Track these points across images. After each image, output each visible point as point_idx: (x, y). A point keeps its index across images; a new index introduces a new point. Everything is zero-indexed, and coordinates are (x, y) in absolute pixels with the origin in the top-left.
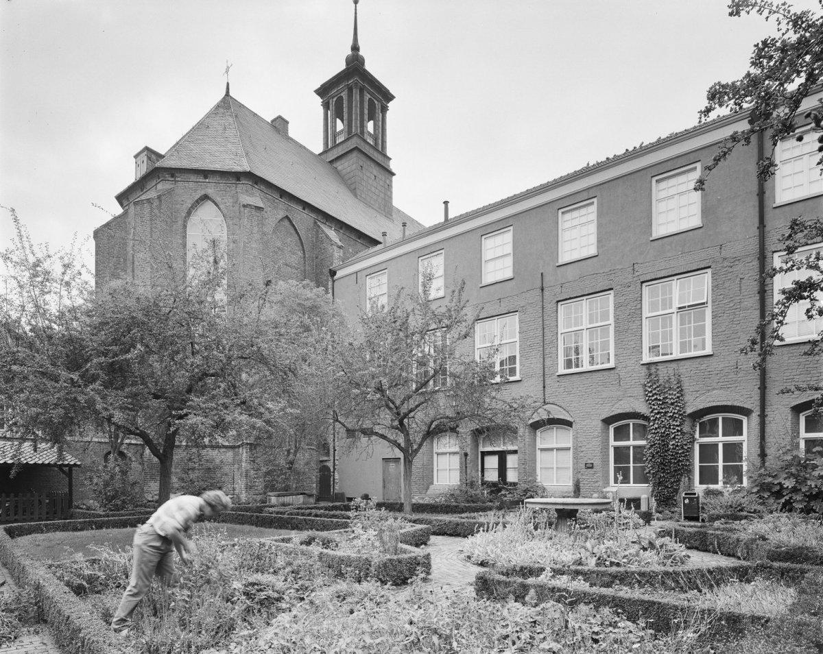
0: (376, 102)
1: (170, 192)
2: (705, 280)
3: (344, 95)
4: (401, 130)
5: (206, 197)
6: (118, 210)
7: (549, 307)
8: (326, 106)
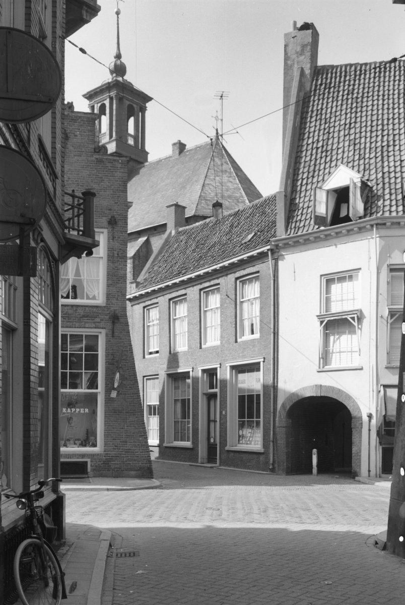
0: (135, 106)
3: (107, 103)
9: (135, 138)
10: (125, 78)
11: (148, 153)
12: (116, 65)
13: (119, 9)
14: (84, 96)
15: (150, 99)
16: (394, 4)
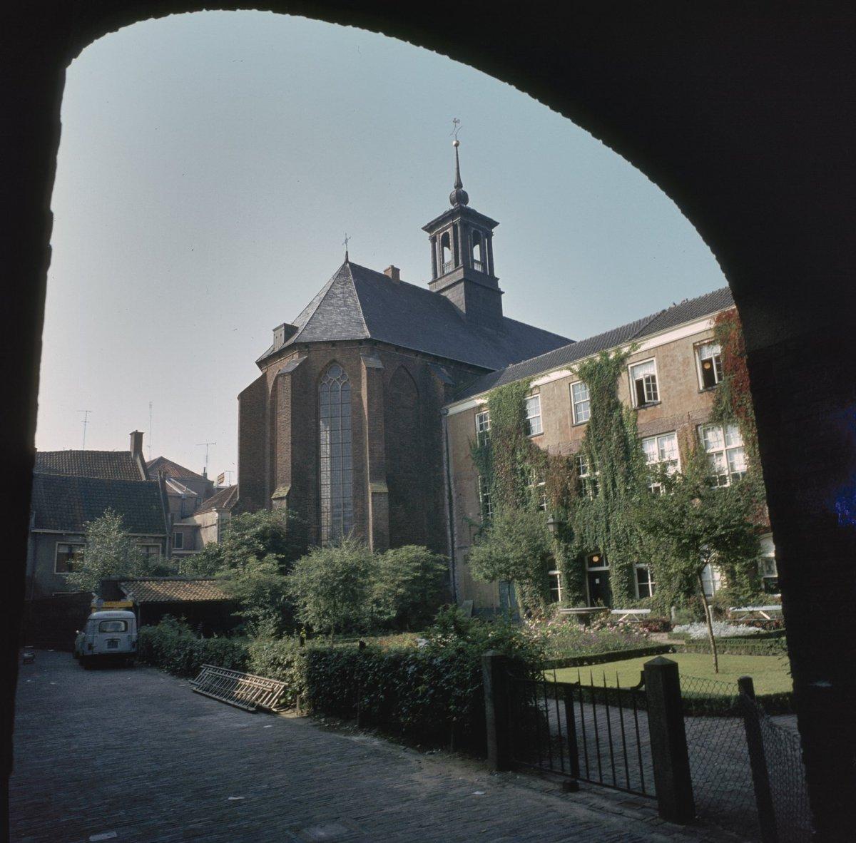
3: (450, 231)
9: (483, 263)
10: (468, 205)
11: (499, 279)
12: (457, 194)
13: (458, 141)
14: (423, 228)
15: (496, 224)
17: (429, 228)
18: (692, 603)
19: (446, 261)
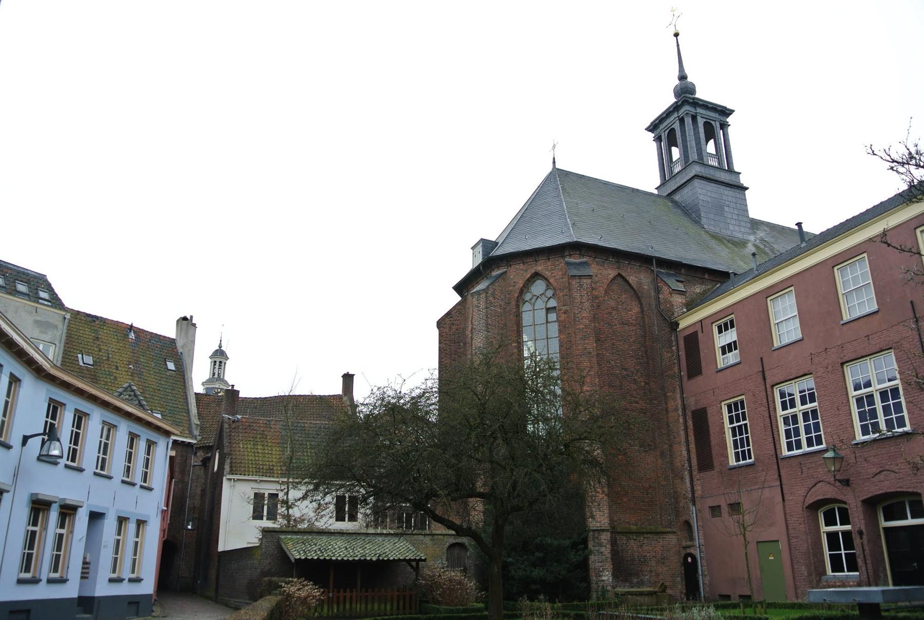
1: (505, 272)
2: (891, 356)
3: (677, 126)
4: (749, 148)
5: (536, 276)
6: (457, 298)
7: (769, 390)
8: (658, 139)
15: (732, 112)
16: (729, 106)
17: (653, 128)
18: (592, 606)
19: (674, 159)
